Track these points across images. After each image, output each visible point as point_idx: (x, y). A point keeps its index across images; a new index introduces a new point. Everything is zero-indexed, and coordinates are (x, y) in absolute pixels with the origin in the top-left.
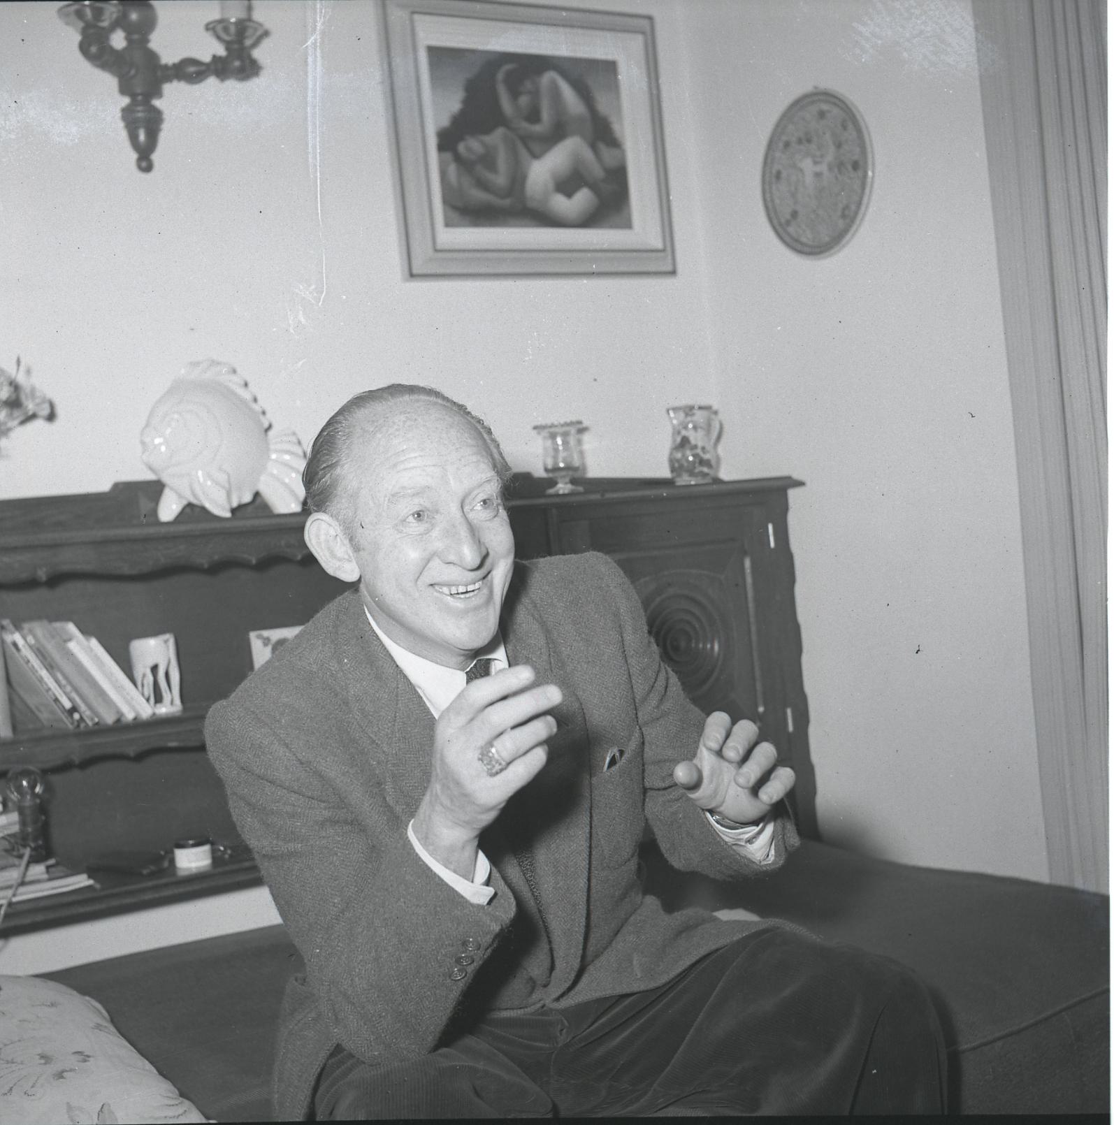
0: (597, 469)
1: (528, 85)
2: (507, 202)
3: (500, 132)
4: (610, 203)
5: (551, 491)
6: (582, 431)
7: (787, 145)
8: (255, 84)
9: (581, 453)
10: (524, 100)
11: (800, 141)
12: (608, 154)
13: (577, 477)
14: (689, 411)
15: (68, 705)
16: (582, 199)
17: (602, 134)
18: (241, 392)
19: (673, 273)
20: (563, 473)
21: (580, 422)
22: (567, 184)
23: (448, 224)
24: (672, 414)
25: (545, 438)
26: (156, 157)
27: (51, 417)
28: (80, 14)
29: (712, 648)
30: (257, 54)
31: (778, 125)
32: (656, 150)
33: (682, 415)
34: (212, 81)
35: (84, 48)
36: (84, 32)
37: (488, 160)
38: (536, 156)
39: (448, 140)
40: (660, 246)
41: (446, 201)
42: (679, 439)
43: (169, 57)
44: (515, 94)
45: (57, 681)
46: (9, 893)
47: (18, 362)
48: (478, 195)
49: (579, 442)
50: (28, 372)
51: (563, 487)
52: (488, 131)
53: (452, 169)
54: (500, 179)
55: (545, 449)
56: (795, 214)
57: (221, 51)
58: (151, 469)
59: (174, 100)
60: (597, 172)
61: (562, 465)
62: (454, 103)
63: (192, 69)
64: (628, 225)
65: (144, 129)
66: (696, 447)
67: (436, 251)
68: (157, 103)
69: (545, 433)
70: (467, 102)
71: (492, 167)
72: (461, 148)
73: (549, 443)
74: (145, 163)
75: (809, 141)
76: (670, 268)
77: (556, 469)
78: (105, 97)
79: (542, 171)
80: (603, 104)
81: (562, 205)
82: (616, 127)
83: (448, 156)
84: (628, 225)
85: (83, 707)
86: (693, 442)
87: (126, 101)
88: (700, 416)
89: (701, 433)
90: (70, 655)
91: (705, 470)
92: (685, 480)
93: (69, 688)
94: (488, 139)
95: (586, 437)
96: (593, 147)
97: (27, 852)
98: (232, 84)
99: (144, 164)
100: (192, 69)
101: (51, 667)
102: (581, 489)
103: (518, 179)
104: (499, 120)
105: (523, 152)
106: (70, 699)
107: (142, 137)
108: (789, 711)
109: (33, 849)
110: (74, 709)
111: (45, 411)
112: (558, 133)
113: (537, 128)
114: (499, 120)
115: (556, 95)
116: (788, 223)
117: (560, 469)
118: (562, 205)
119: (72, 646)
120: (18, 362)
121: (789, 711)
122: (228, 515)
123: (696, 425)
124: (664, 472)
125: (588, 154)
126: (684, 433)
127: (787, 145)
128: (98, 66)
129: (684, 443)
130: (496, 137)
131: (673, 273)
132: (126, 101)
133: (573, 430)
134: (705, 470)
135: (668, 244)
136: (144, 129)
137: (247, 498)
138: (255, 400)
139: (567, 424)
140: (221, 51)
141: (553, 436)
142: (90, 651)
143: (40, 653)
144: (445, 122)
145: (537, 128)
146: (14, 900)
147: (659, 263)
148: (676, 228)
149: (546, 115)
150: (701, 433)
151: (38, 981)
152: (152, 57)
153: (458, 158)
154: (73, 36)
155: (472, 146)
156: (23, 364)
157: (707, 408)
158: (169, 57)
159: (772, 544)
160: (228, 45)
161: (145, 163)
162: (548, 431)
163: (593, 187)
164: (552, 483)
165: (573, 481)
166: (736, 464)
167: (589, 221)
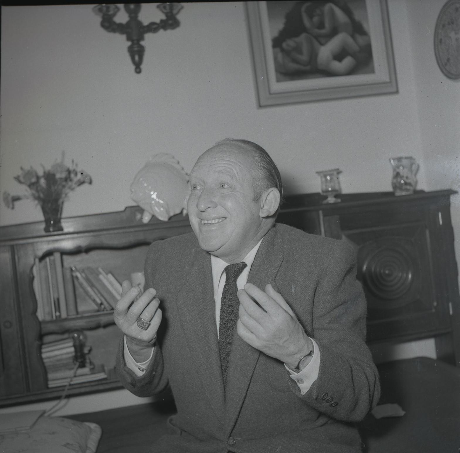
0: (346, 190)
1: (318, 11)
2: (308, 68)
3: (303, 36)
4: (363, 61)
5: (325, 202)
6: (339, 172)
7: (444, 26)
8: (177, 30)
9: (339, 183)
10: (316, 19)
11: (449, 24)
12: (361, 40)
13: (338, 195)
14: (400, 159)
15: (99, 302)
16: (348, 61)
17: (358, 29)
18: (176, 166)
19: (397, 92)
20: (330, 193)
21: (338, 169)
22: (339, 57)
23: (278, 81)
24: (392, 161)
25: (321, 177)
26: (143, 67)
27: (91, 183)
28: (100, 10)
29: (407, 276)
30: (179, 17)
31: (439, 17)
32: (385, 35)
33: (396, 161)
34: (161, 31)
35: (103, 25)
36: (103, 18)
37: (298, 49)
38: (322, 44)
39: (277, 43)
40: (388, 80)
41: (277, 71)
42: (395, 173)
43: (146, 22)
44: (311, 17)
45: (94, 292)
46: (69, 380)
47: (73, 162)
48: (293, 66)
49: (338, 178)
50: (77, 165)
51: (331, 200)
52: (297, 35)
53: (280, 55)
54: (304, 57)
55: (322, 182)
56: (448, 60)
57: (164, 17)
58: (134, 201)
59: (150, 41)
60: (356, 48)
61: (330, 189)
62: (280, 25)
63: (155, 26)
64: (373, 71)
65: (137, 54)
66: (403, 177)
67: (270, 94)
68: (142, 43)
69: (322, 175)
70: (286, 24)
71: (300, 52)
72: (284, 45)
73: (324, 179)
74: (138, 70)
75: (453, 23)
76: (394, 90)
77: (327, 191)
78: (120, 42)
79: (325, 52)
80: (357, 16)
81: (336, 66)
82: (365, 26)
83: (278, 50)
84: (373, 71)
85: (105, 303)
86: (401, 174)
87: (129, 43)
88: (405, 162)
89: (406, 170)
90: (100, 281)
91: (408, 187)
92: (398, 193)
93: (99, 295)
94: (297, 39)
95: (341, 176)
96: (353, 36)
97: (78, 364)
98: (169, 32)
99: (138, 70)
100: (155, 26)
101: (92, 286)
102: (339, 200)
103: (314, 55)
104: (304, 30)
105: (316, 43)
106: (100, 300)
107: (137, 58)
108: (450, 305)
109: (80, 362)
110: (102, 304)
111: (87, 180)
112: (334, 32)
113: (323, 31)
114: (304, 30)
115: (332, 13)
116: (446, 64)
117: (329, 191)
118: (336, 66)
119: (101, 277)
120: (73, 162)
121: (450, 305)
122: (166, 219)
123: (404, 165)
124: (390, 189)
125: (350, 40)
126: (398, 170)
127: (444, 26)
128: (109, 31)
129: (397, 175)
130: (302, 38)
131: (397, 92)
132: (129, 43)
133: (335, 173)
134: (408, 187)
135: (393, 78)
136: (137, 54)
137: (178, 211)
138: (183, 169)
139: (332, 170)
140: (164, 17)
141: (325, 176)
142: (108, 279)
143: (88, 280)
144: (276, 34)
145: (323, 31)
146: (72, 383)
147: (390, 88)
148: (398, 72)
149: (327, 25)
150: (406, 170)
151: (70, 421)
152: (140, 23)
153: (283, 50)
154: (98, 19)
155: (290, 43)
156: (75, 162)
157: (411, 158)
158: (146, 23)
159: (441, 222)
160: (166, 14)
161: (138, 70)
162: (323, 174)
163: (353, 55)
164: (326, 197)
165: (336, 196)
166: (424, 184)
167: (351, 72)
